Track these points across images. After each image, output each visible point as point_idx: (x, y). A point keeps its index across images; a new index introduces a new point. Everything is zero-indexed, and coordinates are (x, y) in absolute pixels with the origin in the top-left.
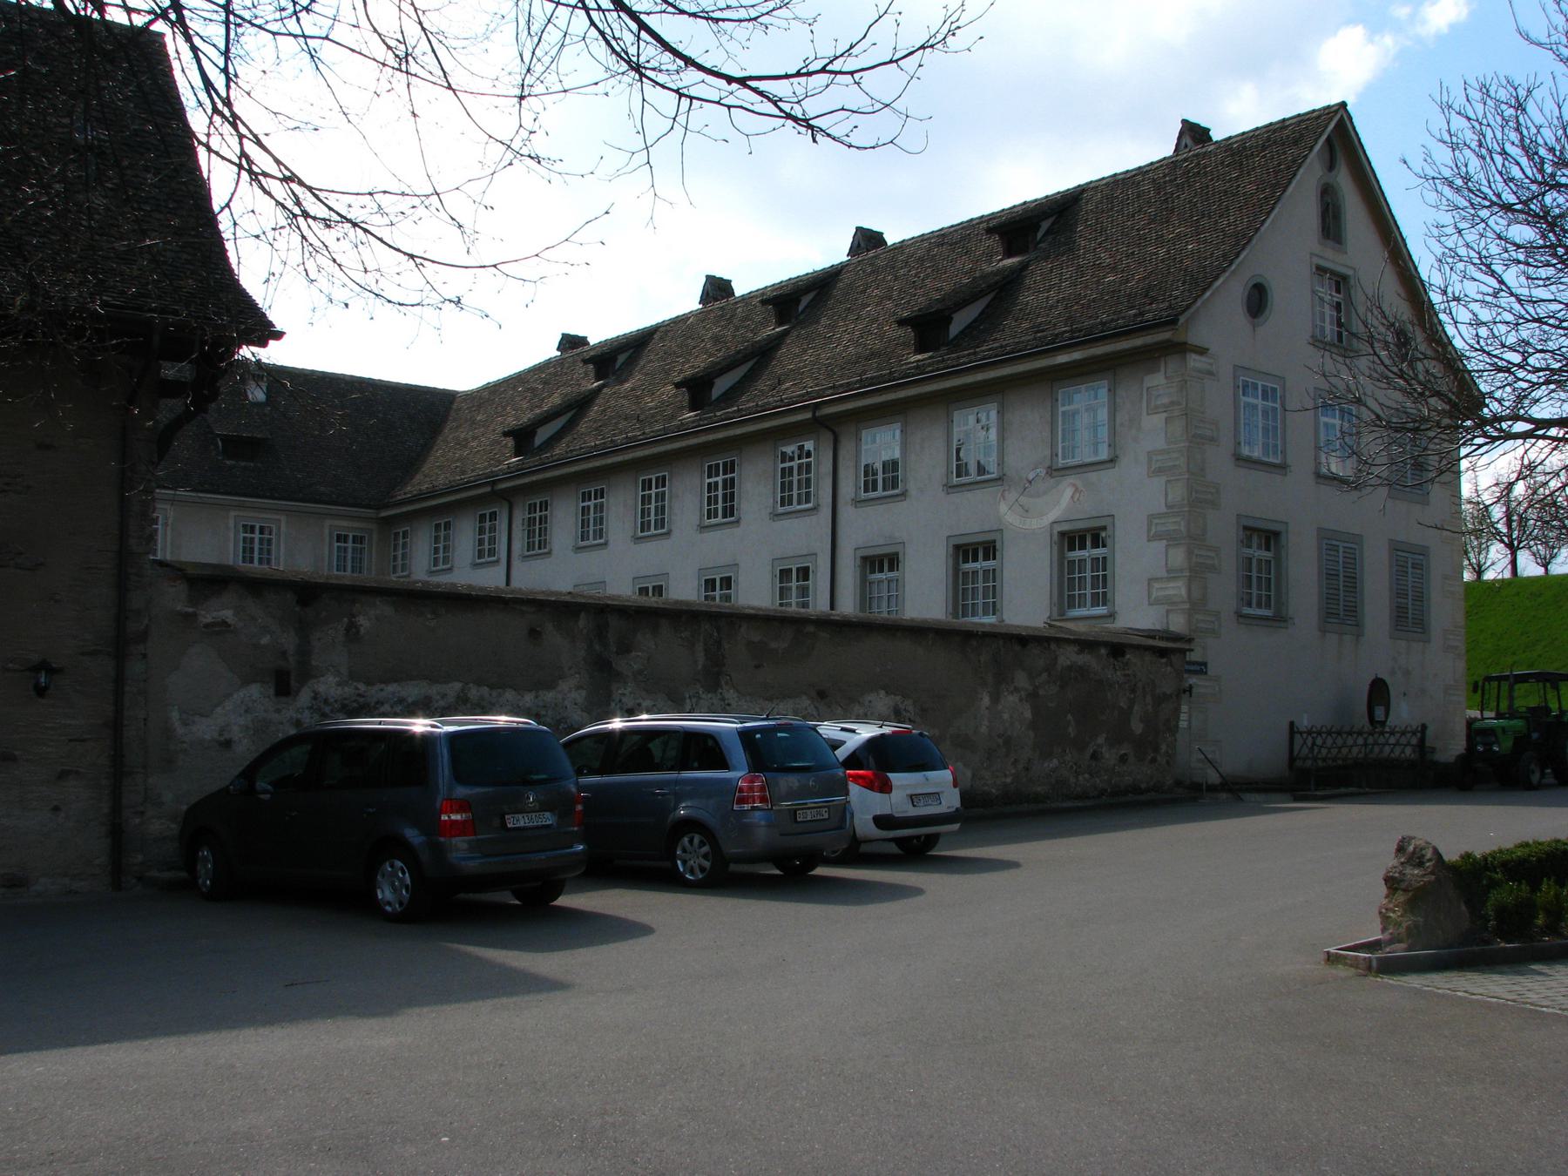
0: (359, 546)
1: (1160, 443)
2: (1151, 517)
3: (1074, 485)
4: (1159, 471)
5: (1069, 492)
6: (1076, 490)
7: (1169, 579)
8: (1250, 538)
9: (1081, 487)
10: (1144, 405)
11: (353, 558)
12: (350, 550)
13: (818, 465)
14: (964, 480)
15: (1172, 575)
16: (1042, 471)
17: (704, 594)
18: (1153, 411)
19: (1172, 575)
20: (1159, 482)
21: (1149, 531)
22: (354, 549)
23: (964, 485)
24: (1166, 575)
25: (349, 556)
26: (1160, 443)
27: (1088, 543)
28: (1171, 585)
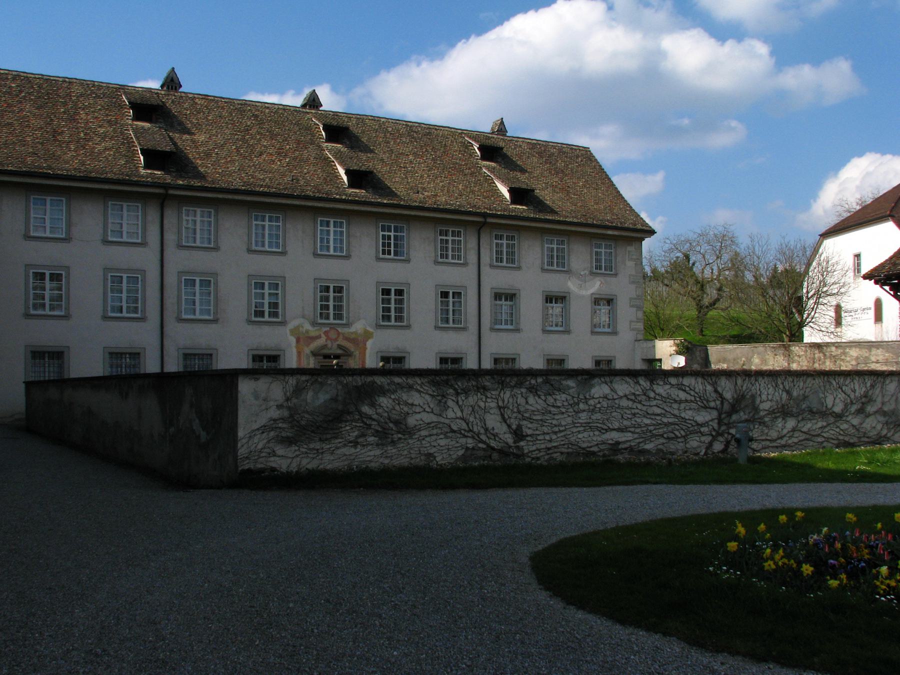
0: (339, 229)
1: (633, 273)
2: (631, 299)
3: (600, 281)
4: (633, 282)
5: (598, 283)
6: (601, 282)
7: (637, 322)
8: (36, 276)
9: (603, 282)
10: (627, 257)
11: (334, 239)
12: (267, 228)
13: (466, 242)
14: (550, 268)
15: (638, 320)
16: (587, 272)
17: (382, 306)
18: (631, 259)
19: (638, 320)
20: (633, 286)
21: (630, 303)
22: (508, 245)
23: (499, 266)
24: (635, 320)
25: (332, 237)
26: (633, 273)
27: (503, 299)
28: (638, 324)
